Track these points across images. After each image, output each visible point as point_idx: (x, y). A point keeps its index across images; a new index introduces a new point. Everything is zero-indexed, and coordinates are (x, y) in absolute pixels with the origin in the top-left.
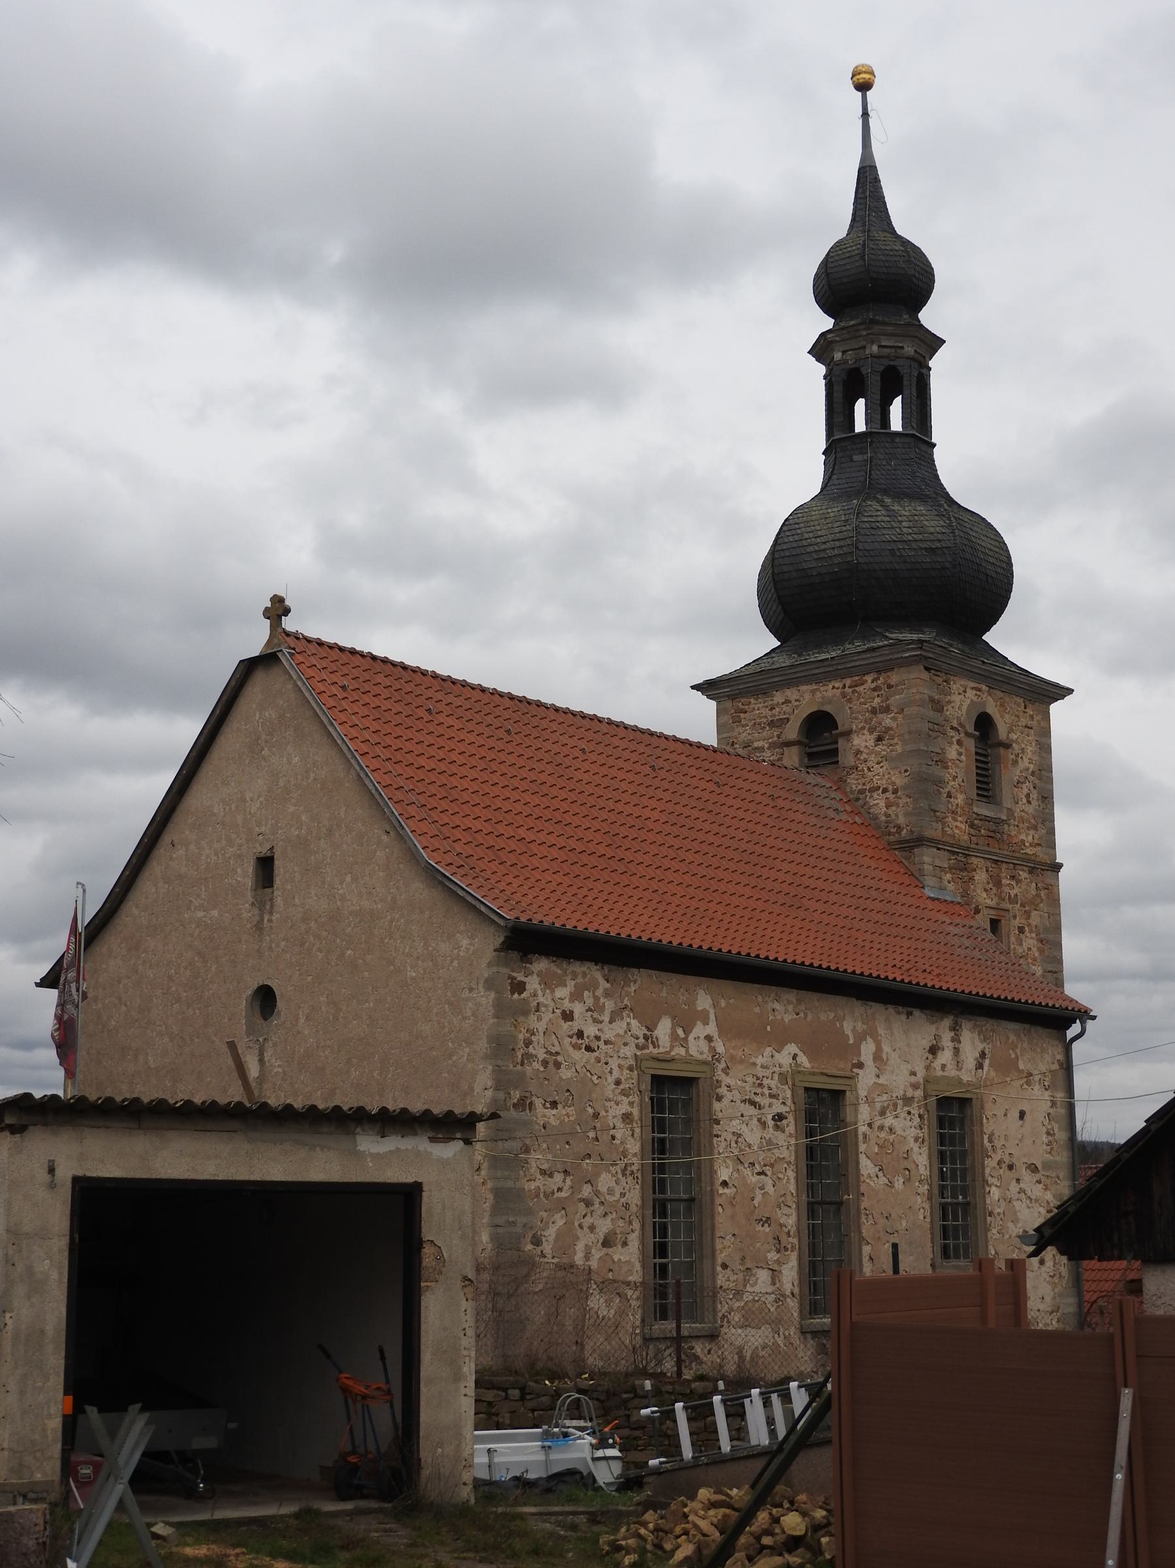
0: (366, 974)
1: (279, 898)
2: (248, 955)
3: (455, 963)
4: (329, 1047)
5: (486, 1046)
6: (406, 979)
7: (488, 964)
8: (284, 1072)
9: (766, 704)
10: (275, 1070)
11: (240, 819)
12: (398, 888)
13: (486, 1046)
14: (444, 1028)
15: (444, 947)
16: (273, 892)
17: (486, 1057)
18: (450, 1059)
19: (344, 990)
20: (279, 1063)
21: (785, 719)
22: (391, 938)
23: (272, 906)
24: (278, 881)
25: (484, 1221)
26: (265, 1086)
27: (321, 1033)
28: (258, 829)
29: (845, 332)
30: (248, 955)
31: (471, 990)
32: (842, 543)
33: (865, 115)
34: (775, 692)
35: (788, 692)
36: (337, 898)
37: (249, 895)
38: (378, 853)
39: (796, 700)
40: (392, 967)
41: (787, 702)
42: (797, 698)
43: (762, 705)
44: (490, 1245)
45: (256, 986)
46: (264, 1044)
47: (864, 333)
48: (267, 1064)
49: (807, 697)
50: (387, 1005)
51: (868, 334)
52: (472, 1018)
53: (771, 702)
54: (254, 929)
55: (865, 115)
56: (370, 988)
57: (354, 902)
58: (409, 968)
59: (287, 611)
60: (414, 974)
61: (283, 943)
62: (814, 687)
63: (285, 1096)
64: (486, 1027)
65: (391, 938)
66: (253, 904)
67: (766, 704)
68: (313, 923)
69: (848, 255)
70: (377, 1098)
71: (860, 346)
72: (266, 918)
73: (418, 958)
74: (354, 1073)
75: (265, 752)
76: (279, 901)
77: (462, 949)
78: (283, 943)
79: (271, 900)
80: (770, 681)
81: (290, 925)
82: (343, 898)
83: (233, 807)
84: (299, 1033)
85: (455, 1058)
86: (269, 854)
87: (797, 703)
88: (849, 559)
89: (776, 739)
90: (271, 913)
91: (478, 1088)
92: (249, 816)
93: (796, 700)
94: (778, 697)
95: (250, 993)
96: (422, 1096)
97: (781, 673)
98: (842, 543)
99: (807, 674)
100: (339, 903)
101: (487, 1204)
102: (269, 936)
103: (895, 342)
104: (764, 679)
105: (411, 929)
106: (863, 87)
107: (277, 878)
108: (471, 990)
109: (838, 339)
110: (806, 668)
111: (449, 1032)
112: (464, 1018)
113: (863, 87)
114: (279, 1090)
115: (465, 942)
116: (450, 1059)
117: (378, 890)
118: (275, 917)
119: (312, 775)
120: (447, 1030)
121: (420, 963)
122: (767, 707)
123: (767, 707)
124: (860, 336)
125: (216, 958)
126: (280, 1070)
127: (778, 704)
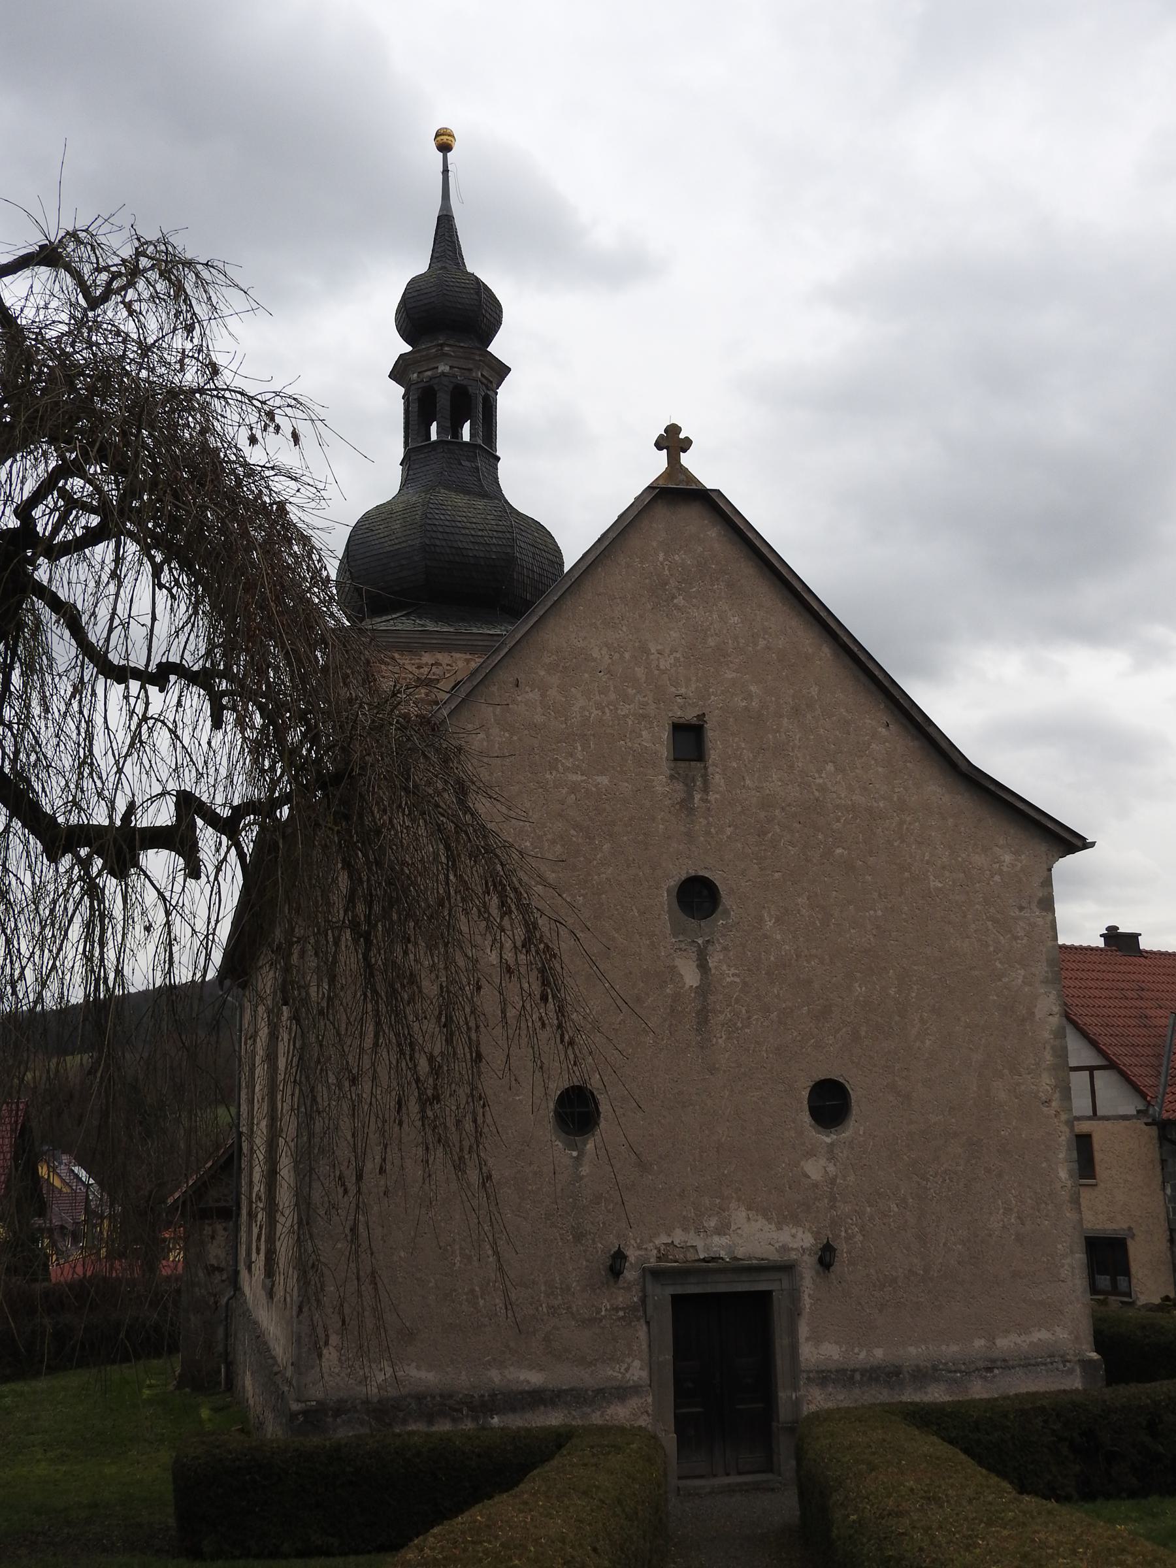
0: (869, 878)
1: (717, 777)
2: (669, 838)
3: (997, 878)
4: (816, 956)
5: (1046, 969)
6: (929, 889)
7: (1042, 883)
8: (745, 984)
9: (413, 662)
10: (728, 980)
11: (640, 672)
12: (906, 789)
13: (1046, 969)
14: (987, 946)
15: (979, 860)
16: (706, 768)
17: (1046, 982)
18: (1000, 980)
19: (834, 893)
20: (733, 971)
21: (435, 679)
22: (903, 841)
23: (706, 782)
24: (713, 755)
25: (1061, 1156)
26: (712, 998)
27: (801, 939)
28: (673, 689)
29: (461, 350)
30: (669, 838)
31: (1021, 908)
32: (500, 535)
33: (446, 171)
34: (423, 653)
35: (439, 656)
36: (814, 787)
37: (665, 767)
38: (873, 746)
39: (448, 665)
40: (907, 874)
41: (437, 664)
42: (449, 663)
43: (408, 661)
44: (1069, 1182)
45: (684, 876)
46: (706, 948)
47: (477, 358)
48: (713, 971)
49: (461, 664)
50: (904, 916)
51: (480, 360)
52: (1026, 938)
53: (417, 661)
54: (678, 807)
55: (446, 171)
56: (876, 894)
57: (843, 796)
58: (932, 877)
59: (686, 444)
60: (940, 885)
61: (729, 831)
62: (468, 656)
63: (747, 1012)
64: (1044, 950)
65: (903, 841)
66: (672, 777)
67: (413, 662)
68: (777, 812)
69: (463, 285)
70: (897, 1018)
71: (467, 367)
72: (697, 797)
73: (944, 868)
74: (859, 989)
75: (680, 601)
76: (717, 779)
77: (1005, 864)
78: (729, 831)
79: (705, 777)
80: (421, 641)
81: (739, 809)
82: (823, 789)
83: (627, 655)
84: (766, 937)
85: (1005, 980)
86: (695, 721)
87: (449, 668)
88: (509, 551)
89: (423, 696)
90: (706, 789)
91: (1039, 1013)
92: (656, 672)
93: (448, 665)
94: (427, 658)
95: (672, 883)
96: (963, 1019)
97: (445, 637)
98: (500, 535)
99: (470, 643)
100: (817, 794)
101: (1063, 1138)
102: (706, 818)
103: (490, 376)
104: (420, 638)
105: (930, 835)
106: (445, 148)
107: (712, 752)
108: (1021, 908)
109: (452, 354)
110: (473, 638)
111: (994, 951)
112: (1016, 938)
113: (445, 148)
114: (736, 1003)
115: (1008, 858)
116: (1000, 980)
117: (877, 786)
118: (712, 797)
119: (762, 643)
120: (992, 949)
121: (947, 874)
122: (413, 664)
123: (413, 664)
124: (474, 359)
125: (611, 836)
126: (737, 980)
127: (427, 664)
